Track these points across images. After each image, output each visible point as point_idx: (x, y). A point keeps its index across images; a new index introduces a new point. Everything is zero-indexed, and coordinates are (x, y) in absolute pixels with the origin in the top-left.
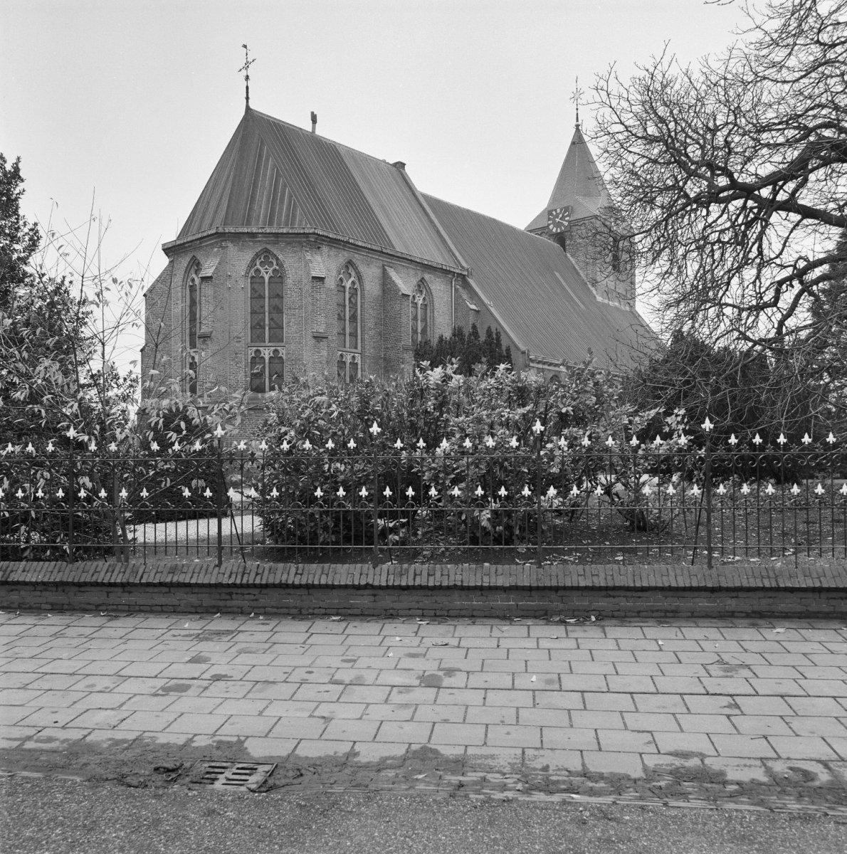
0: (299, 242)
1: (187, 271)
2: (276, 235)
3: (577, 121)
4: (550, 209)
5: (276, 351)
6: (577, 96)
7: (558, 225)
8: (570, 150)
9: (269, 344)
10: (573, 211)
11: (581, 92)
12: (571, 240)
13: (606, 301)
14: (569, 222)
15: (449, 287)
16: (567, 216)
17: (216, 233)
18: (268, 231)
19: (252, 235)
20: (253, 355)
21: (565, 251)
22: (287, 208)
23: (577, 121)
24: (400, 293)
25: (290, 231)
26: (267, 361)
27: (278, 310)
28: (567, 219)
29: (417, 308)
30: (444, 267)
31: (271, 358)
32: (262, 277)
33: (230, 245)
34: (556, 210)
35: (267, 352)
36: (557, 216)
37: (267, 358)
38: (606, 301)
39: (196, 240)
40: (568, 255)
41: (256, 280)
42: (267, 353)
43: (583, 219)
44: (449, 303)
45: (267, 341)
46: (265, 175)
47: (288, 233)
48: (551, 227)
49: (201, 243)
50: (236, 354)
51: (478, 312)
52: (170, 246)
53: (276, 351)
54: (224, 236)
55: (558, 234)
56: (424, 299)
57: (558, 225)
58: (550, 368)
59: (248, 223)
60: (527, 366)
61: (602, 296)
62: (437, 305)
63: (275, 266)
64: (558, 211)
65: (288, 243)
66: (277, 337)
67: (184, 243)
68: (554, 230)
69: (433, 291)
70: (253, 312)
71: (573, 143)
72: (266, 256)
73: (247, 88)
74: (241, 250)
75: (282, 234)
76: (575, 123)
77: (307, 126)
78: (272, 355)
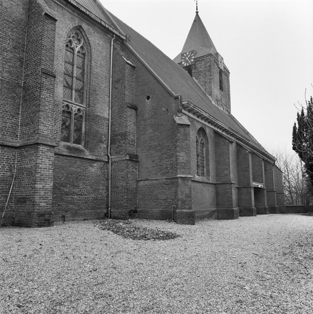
4: (183, 53)
8: (193, 23)
10: (196, 53)
12: (195, 69)
13: (217, 106)
14: (194, 59)
15: (108, 45)
16: (193, 56)
21: (191, 76)
24: (43, 13)
28: (193, 57)
29: (74, 54)
30: (103, 23)
34: (186, 53)
38: (217, 106)
40: (194, 78)
43: (203, 57)
44: (108, 59)
48: (183, 63)
51: (134, 67)
55: (187, 67)
56: (82, 47)
57: (187, 62)
58: (199, 120)
60: (180, 111)
61: (215, 102)
62: (94, 55)
64: (188, 53)
68: (185, 65)
69: (92, 44)
71: (195, 21)
76: (196, 11)
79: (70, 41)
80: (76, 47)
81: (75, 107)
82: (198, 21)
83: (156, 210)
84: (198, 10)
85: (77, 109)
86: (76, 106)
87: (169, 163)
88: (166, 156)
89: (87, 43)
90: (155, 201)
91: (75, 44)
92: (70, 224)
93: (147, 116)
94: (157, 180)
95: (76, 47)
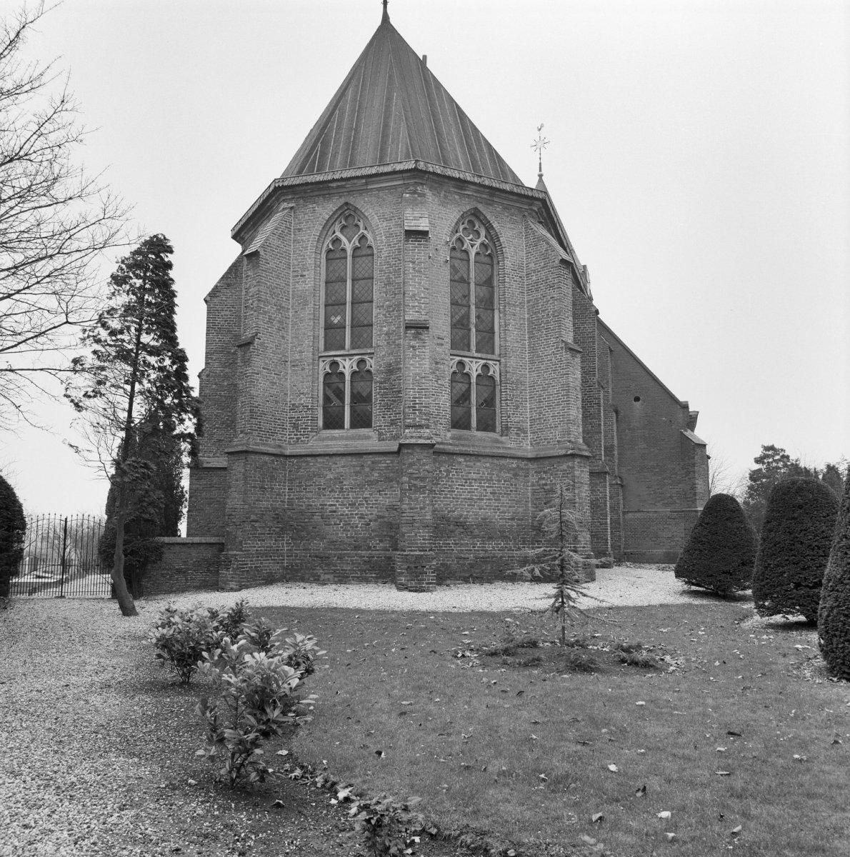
1: (327, 225)
3: (540, 170)
6: (540, 144)
9: (476, 355)
11: (546, 141)
17: (415, 169)
19: (461, 184)
20: (480, 371)
23: (540, 170)
25: (515, 190)
26: (474, 380)
27: (487, 304)
33: (427, 191)
35: (474, 366)
39: (362, 177)
41: (334, 255)
42: (474, 368)
45: (473, 347)
49: (367, 184)
50: (437, 363)
52: (256, 206)
53: (486, 367)
54: (422, 178)
59: (320, 170)
63: (482, 238)
65: (506, 208)
66: (486, 343)
67: (330, 181)
70: (454, 303)
72: (474, 218)
74: (443, 204)
76: (537, 172)
78: (328, 370)
79: (460, 240)
80: (472, 246)
81: (476, 362)
83: (659, 551)
84: (543, 172)
85: (480, 367)
86: (477, 360)
87: (674, 491)
88: (670, 482)
89: (493, 237)
90: (654, 539)
91: (468, 241)
92: (472, 585)
94: (656, 512)
95: (472, 246)
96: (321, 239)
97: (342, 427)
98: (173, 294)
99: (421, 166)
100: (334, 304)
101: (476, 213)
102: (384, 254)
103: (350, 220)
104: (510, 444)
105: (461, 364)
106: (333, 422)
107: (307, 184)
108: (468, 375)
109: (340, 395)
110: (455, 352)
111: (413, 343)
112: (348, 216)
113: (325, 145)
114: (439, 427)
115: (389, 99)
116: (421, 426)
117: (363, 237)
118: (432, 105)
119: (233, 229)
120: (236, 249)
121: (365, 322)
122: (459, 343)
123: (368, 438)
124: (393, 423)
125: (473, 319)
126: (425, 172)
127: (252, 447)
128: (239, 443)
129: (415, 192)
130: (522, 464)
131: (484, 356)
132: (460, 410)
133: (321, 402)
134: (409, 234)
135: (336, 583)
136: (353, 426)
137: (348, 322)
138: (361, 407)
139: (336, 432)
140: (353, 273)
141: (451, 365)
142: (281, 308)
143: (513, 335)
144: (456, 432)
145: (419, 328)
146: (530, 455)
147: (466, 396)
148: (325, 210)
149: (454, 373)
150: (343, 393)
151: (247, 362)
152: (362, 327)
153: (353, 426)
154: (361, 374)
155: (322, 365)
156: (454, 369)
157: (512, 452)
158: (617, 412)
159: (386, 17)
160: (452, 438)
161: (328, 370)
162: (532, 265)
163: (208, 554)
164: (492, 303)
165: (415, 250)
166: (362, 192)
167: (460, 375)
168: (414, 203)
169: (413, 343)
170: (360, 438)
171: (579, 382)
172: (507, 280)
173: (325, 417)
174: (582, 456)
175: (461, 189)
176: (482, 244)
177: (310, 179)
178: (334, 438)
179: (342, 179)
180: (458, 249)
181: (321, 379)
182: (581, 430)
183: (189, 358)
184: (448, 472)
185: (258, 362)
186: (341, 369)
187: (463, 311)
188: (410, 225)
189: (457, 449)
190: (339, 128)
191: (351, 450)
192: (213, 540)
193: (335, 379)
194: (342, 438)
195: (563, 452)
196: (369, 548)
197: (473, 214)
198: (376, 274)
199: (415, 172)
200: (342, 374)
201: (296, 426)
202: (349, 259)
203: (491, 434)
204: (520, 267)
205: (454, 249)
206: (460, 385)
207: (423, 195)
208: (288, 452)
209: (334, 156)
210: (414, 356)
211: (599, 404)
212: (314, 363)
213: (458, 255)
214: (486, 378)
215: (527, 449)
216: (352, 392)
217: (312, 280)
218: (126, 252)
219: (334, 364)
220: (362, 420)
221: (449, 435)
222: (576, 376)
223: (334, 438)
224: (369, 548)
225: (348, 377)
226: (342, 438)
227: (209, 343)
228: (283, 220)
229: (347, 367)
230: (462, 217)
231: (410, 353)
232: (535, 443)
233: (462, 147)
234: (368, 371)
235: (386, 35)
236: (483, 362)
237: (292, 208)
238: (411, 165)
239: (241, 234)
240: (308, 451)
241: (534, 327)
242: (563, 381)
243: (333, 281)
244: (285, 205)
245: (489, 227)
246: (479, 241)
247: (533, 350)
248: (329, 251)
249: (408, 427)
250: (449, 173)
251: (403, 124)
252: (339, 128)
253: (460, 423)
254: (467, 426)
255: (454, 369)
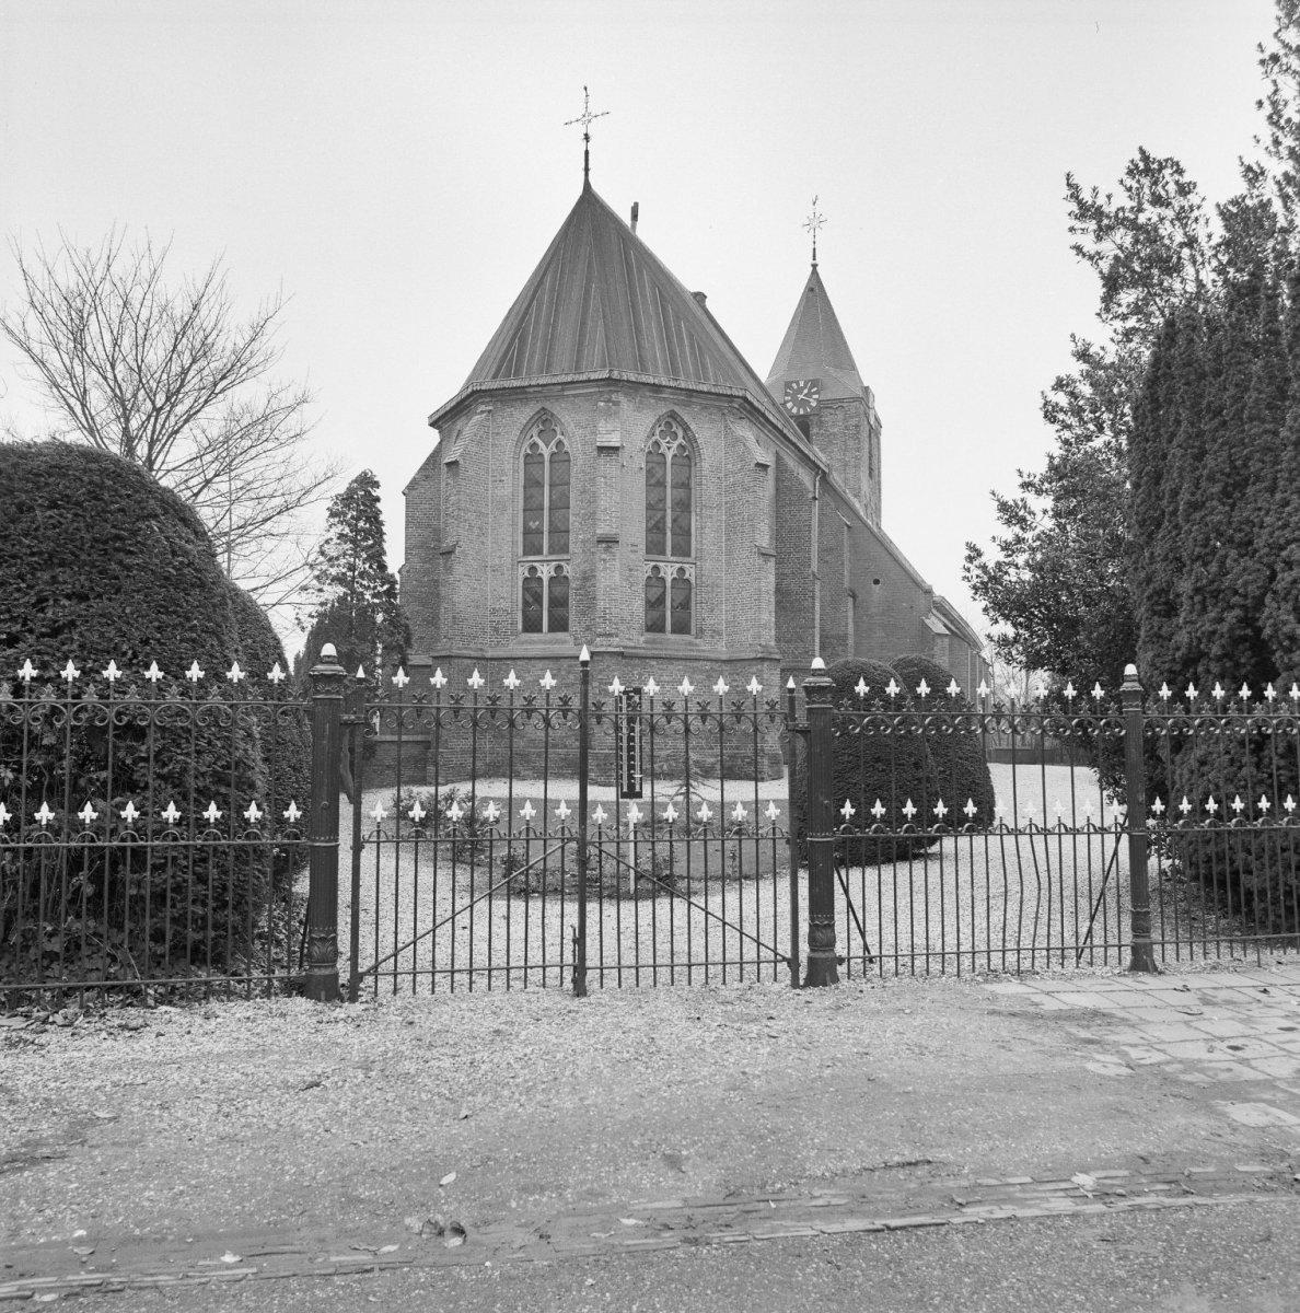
0: (719, 408)
1: (525, 430)
2: (690, 392)
5: (681, 570)
7: (803, 403)
9: (671, 559)
14: (818, 401)
16: (815, 393)
17: (609, 379)
18: (683, 386)
19: (657, 388)
22: (522, 362)
26: (669, 584)
27: (684, 506)
31: (551, 578)
32: (663, 455)
33: (621, 398)
34: (797, 383)
36: (800, 390)
37: (669, 580)
41: (533, 459)
46: (644, 296)
47: (709, 393)
48: (789, 405)
49: (563, 390)
50: (631, 570)
52: (454, 403)
53: (681, 570)
55: (797, 418)
59: (517, 373)
63: (680, 440)
64: (802, 384)
66: (682, 550)
68: (795, 411)
70: (650, 507)
73: (587, 153)
74: (638, 409)
75: (702, 392)
77: (626, 219)
78: (527, 574)
79: (657, 443)
82: (815, 291)
84: (817, 262)
93: (874, 610)
96: (519, 443)
97: (540, 631)
98: (381, 524)
99: (615, 375)
100: (532, 509)
101: (673, 415)
102: (580, 462)
103: (547, 424)
104: (704, 646)
105: (656, 568)
106: (532, 625)
107: (504, 388)
108: (663, 580)
109: (538, 599)
110: (651, 557)
111: (604, 556)
112: (545, 422)
113: (523, 341)
114: (633, 632)
115: (587, 292)
116: (610, 635)
117: (560, 443)
118: (633, 294)
119: (431, 417)
120: (434, 437)
121: (563, 529)
122: (655, 547)
123: (564, 642)
124: (588, 628)
125: (669, 524)
126: (619, 381)
127: (455, 652)
128: (442, 648)
129: (609, 401)
130: (716, 666)
131: (680, 559)
132: (655, 614)
133: (520, 606)
134: (601, 449)
135: (535, 778)
136: (551, 629)
137: (546, 528)
138: (560, 611)
139: (535, 636)
140: (551, 478)
141: (646, 570)
142: (480, 515)
143: (710, 535)
144: (650, 635)
145: (609, 542)
146: (724, 657)
147: (661, 600)
148: (523, 414)
149: (649, 578)
150: (541, 597)
151: (449, 570)
152: (560, 532)
153: (551, 629)
154: (559, 579)
155: (520, 569)
156: (649, 574)
157: (706, 654)
158: (854, 597)
159: (587, 185)
160: (646, 642)
161: (527, 574)
162: (730, 466)
163: (415, 751)
164: (689, 506)
165: (607, 466)
166: (560, 397)
167: (655, 579)
168: (608, 414)
169: (604, 556)
170: (557, 642)
171: (772, 587)
172: (704, 482)
173: (524, 621)
174: (771, 659)
175: (656, 392)
176: (680, 445)
177: (506, 384)
178: (534, 642)
179: (538, 385)
180: (654, 456)
181: (520, 584)
182: (773, 632)
183: (355, 473)
184: (640, 675)
185: (459, 569)
186: (539, 574)
187: (659, 515)
188: (603, 441)
189: (649, 653)
190: (537, 322)
191: (548, 654)
192: (419, 738)
193: (534, 584)
194: (541, 642)
195: (753, 655)
196: (566, 747)
197: (671, 416)
198: (572, 480)
199: (609, 381)
200: (540, 579)
201: (496, 630)
202: (547, 464)
203: (686, 637)
204: (718, 469)
205: (650, 452)
206: (655, 589)
207: (617, 403)
208: (489, 655)
209: (532, 356)
210: (605, 569)
211: (813, 598)
212: (513, 568)
213: (655, 458)
214: (681, 581)
215: (722, 650)
216: (550, 598)
217: (511, 486)
218: (342, 489)
219: (533, 570)
220: (559, 625)
221: (642, 639)
222: (769, 581)
223: (534, 642)
224: (566, 747)
225: (546, 583)
226: (541, 642)
227: (408, 537)
228: (481, 424)
229: (545, 572)
230: (658, 420)
231: (600, 566)
232: (730, 645)
233: (662, 341)
234: (566, 577)
235: (589, 206)
236: (678, 565)
237: (490, 411)
238: (605, 375)
239: (444, 420)
240: (508, 654)
241: (731, 530)
242: (756, 586)
243: (532, 484)
244: (483, 408)
245: (686, 429)
246: (677, 443)
247: (729, 553)
248: (527, 456)
249: (600, 635)
250: (644, 379)
251: (601, 322)
252: (537, 322)
253: (655, 626)
254: (662, 629)
255: (649, 574)
